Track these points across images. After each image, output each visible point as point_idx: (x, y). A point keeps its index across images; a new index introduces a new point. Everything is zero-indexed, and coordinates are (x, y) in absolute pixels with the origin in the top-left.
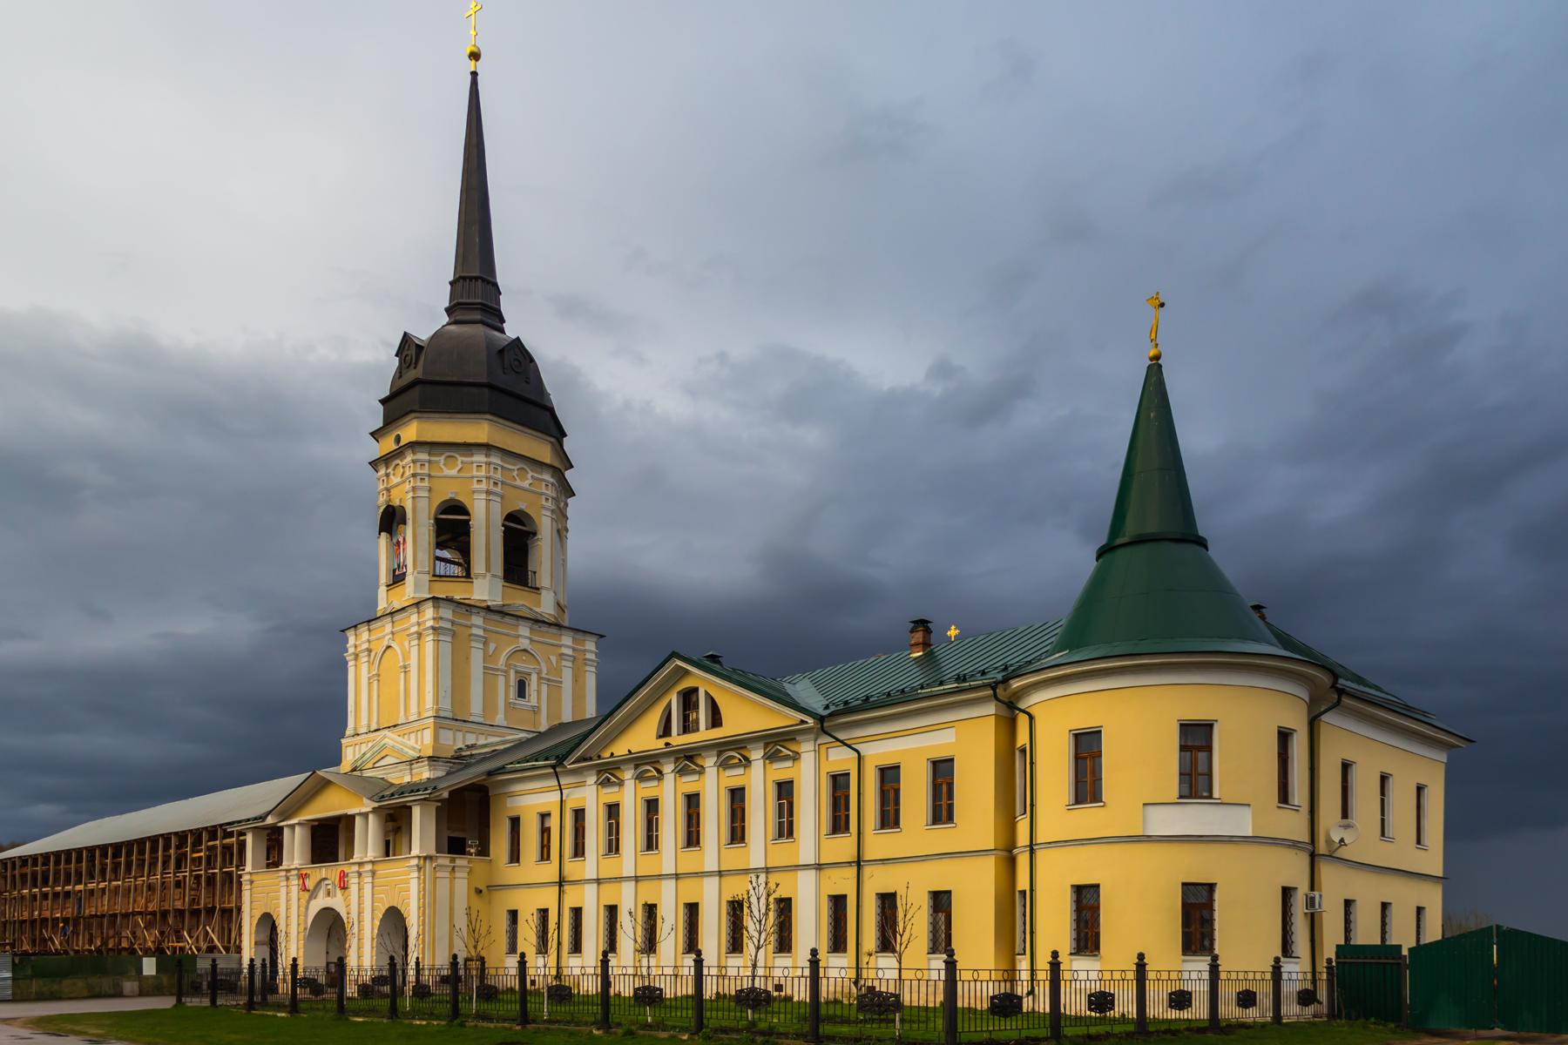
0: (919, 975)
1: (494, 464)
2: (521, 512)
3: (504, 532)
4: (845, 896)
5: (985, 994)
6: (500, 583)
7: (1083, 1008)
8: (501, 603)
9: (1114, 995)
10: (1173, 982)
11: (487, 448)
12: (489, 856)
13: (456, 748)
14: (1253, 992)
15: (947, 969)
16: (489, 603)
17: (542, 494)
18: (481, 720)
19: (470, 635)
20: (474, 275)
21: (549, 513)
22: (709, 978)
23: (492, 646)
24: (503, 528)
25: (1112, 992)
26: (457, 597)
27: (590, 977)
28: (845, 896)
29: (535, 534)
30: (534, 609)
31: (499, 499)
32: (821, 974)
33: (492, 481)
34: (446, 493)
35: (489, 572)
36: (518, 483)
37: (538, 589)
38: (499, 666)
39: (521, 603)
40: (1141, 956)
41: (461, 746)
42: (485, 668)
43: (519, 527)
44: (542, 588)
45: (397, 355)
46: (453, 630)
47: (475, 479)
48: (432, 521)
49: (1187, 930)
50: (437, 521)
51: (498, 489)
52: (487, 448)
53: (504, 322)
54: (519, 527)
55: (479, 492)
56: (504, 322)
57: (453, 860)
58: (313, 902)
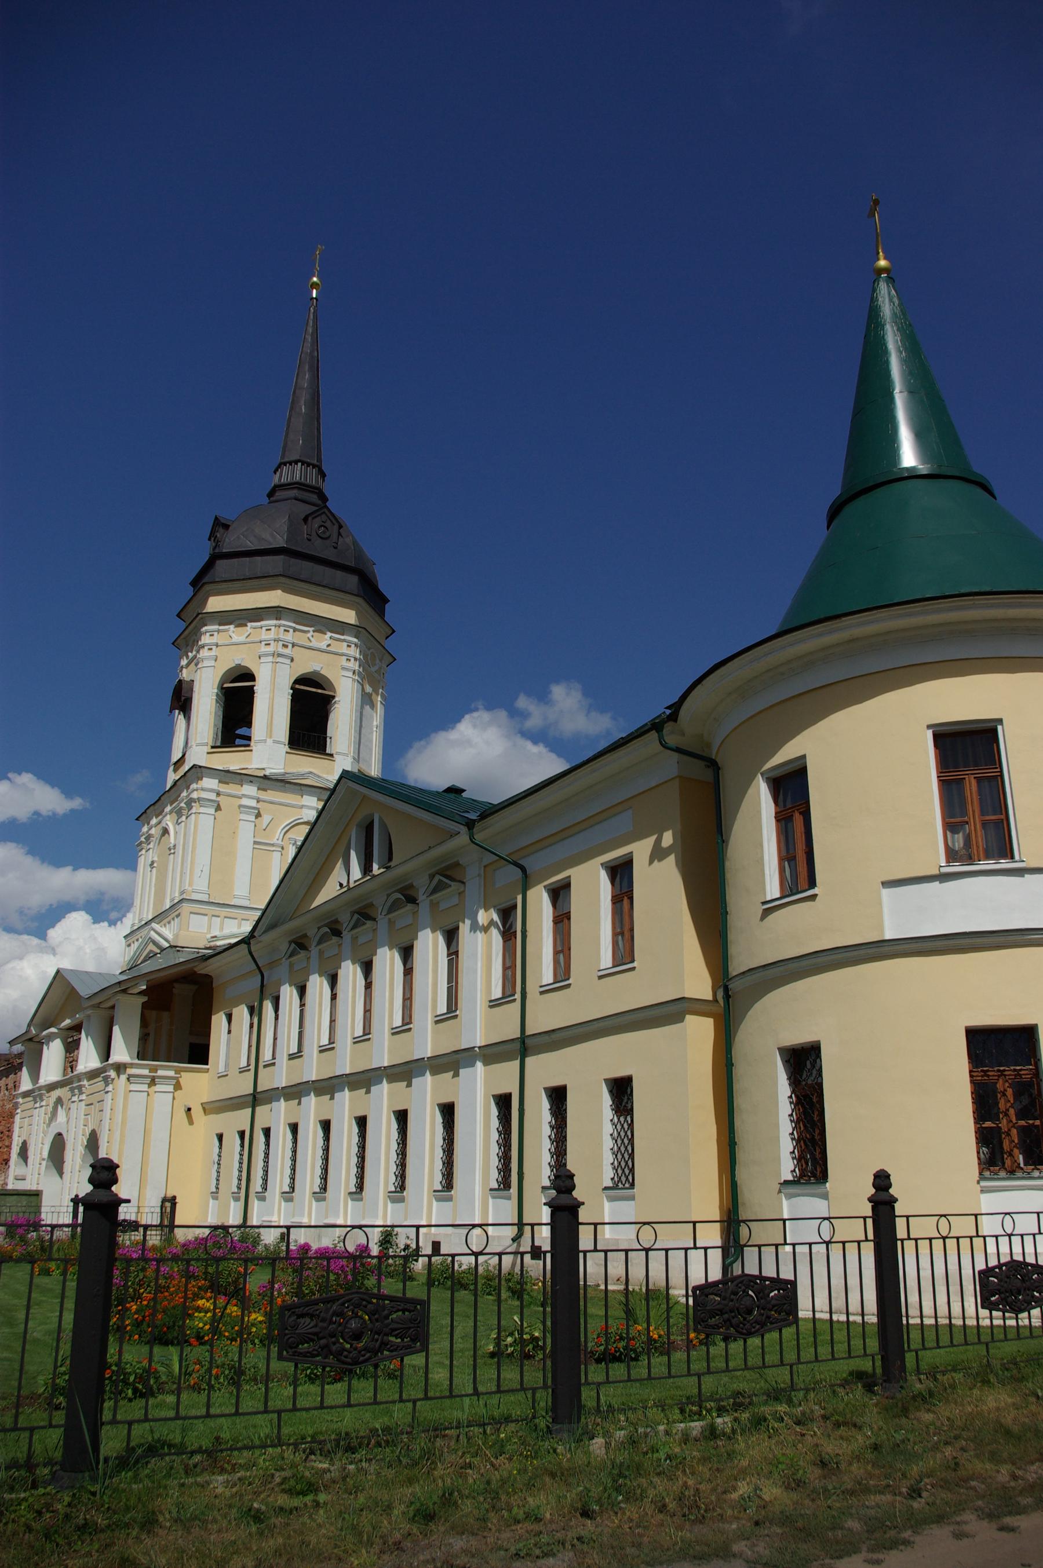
0: (647, 1237)
1: (284, 626)
2: (316, 673)
3: (292, 696)
4: (510, 1095)
5: (967, 1272)
6: (287, 748)
7: (970, 1310)
8: (283, 771)
9: (794, 1283)
10: (924, 1245)
11: (277, 612)
12: (207, 1064)
13: (209, 936)
14: (777, 1282)
15: (553, 1224)
16: (267, 773)
17: (343, 655)
18: (246, 903)
19: (240, 806)
20: (312, 462)
21: (350, 674)
22: (909, 1245)
23: (266, 819)
24: (291, 691)
25: (787, 1274)
26: (232, 768)
27: (852, 1250)
28: (510, 1095)
29: (333, 697)
30: (325, 776)
31: (288, 661)
32: (901, 1233)
33: (281, 643)
34: (308, 664)
35: (271, 737)
36: (314, 643)
37: (331, 755)
38: (275, 841)
39: (307, 770)
40: (882, 1181)
41: (217, 933)
42: (255, 843)
43: (320, 691)
44: (338, 753)
45: (209, 539)
46: (258, 809)
47: (263, 643)
48: (216, 691)
49: (988, 1124)
50: (221, 688)
51: (287, 651)
52: (277, 612)
53: (327, 500)
54: (320, 691)
55: (266, 655)
56: (327, 500)
57: (154, 1069)
58: (50, 1129)
